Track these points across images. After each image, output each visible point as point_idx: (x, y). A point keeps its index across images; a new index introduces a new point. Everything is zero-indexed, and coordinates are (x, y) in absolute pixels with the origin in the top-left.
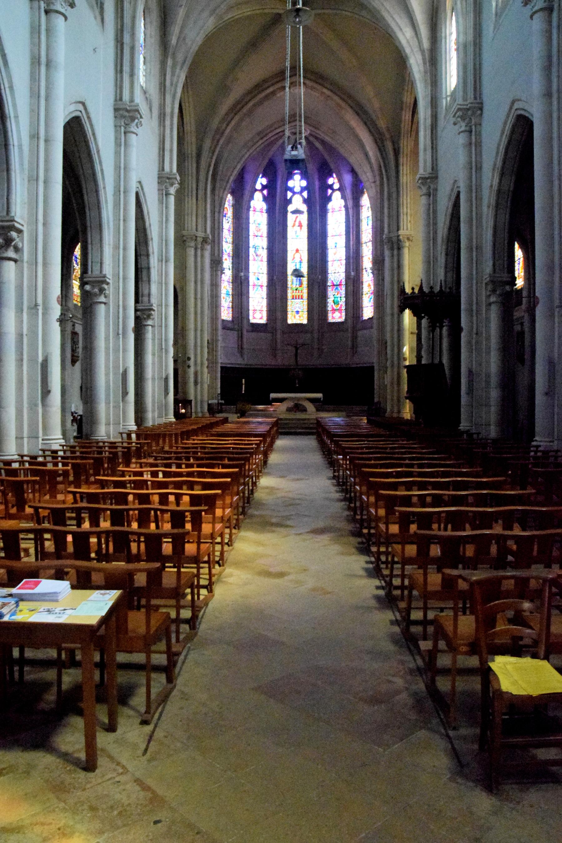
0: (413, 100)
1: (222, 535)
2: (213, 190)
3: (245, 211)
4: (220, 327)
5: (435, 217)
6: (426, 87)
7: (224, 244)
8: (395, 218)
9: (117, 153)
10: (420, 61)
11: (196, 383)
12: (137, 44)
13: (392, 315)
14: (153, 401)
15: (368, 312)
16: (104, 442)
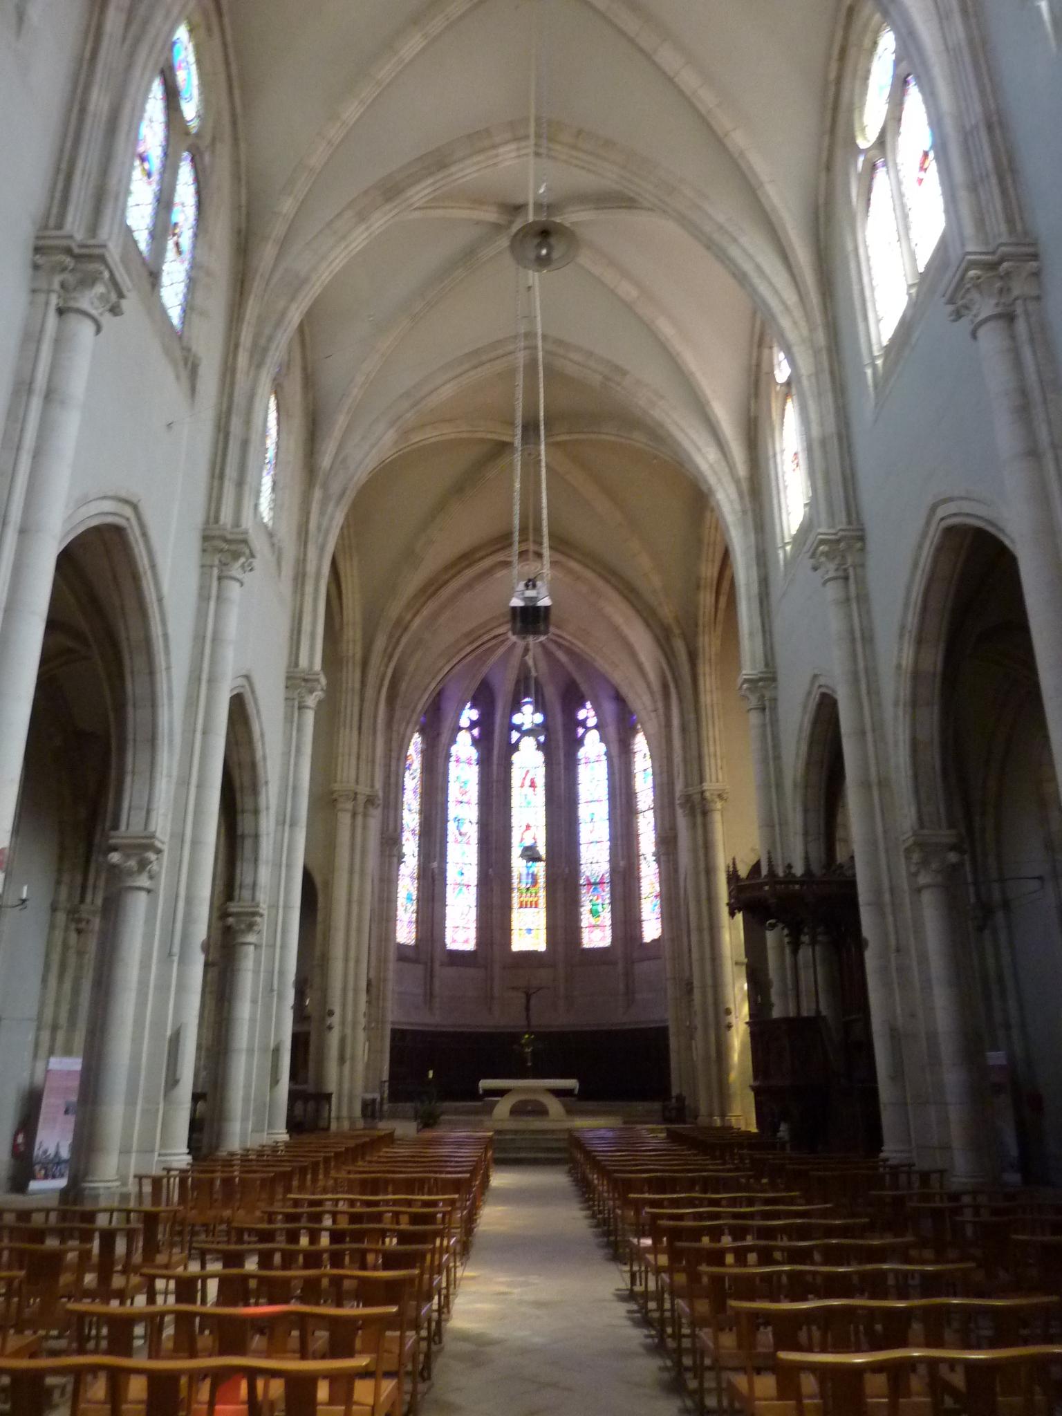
3: (441, 761)
4: (392, 955)
5: (776, 746)
6: (746, 534)
7: (406, 814)
8: (696, 766)
9: (201, 615)
11: (342, 1059)
14: (246, 1100)
15: (651, 929)
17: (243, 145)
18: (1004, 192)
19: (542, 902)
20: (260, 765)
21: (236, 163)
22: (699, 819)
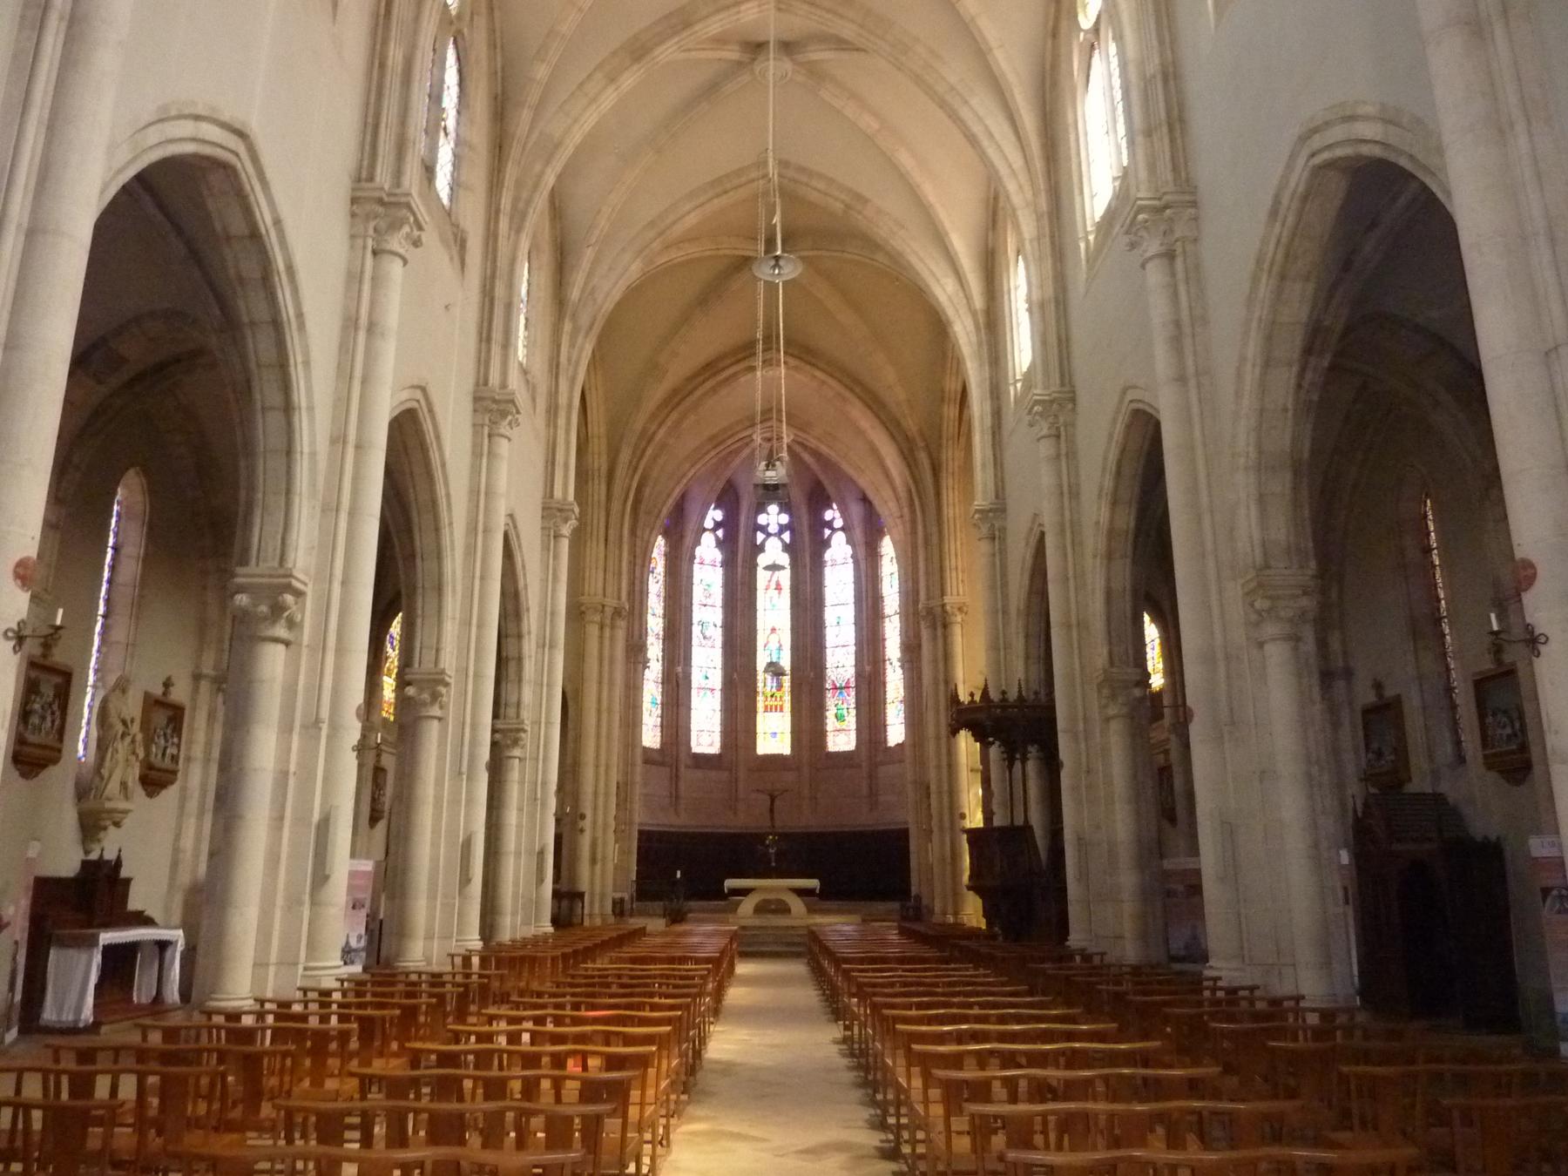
0: (960, 389)
1: (653, 1126)
2: (633, 532)
3: (685, 566)
4: (639, 760)
5: (1004, 575)
7: (650, 618)
8: (937, 577)
9: (475, 470)
10: (971, 327)
11: (593, 861)
12: (516, 300)
13: (938, 738)
15: (896, 733)
16: (420, 974)
17: (497, 14)
18: (1172, 141)
19: (787, 707)
20: (522, 593)
21: (492, 31)
22: (940, 632)
